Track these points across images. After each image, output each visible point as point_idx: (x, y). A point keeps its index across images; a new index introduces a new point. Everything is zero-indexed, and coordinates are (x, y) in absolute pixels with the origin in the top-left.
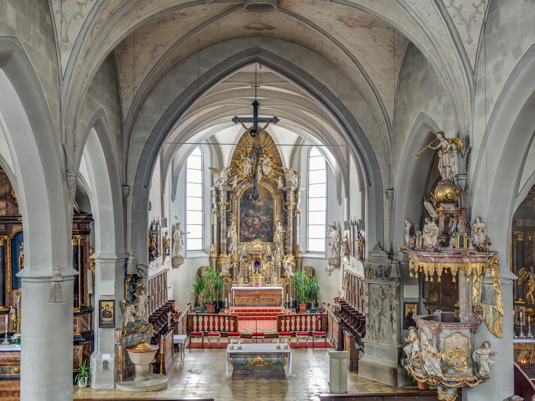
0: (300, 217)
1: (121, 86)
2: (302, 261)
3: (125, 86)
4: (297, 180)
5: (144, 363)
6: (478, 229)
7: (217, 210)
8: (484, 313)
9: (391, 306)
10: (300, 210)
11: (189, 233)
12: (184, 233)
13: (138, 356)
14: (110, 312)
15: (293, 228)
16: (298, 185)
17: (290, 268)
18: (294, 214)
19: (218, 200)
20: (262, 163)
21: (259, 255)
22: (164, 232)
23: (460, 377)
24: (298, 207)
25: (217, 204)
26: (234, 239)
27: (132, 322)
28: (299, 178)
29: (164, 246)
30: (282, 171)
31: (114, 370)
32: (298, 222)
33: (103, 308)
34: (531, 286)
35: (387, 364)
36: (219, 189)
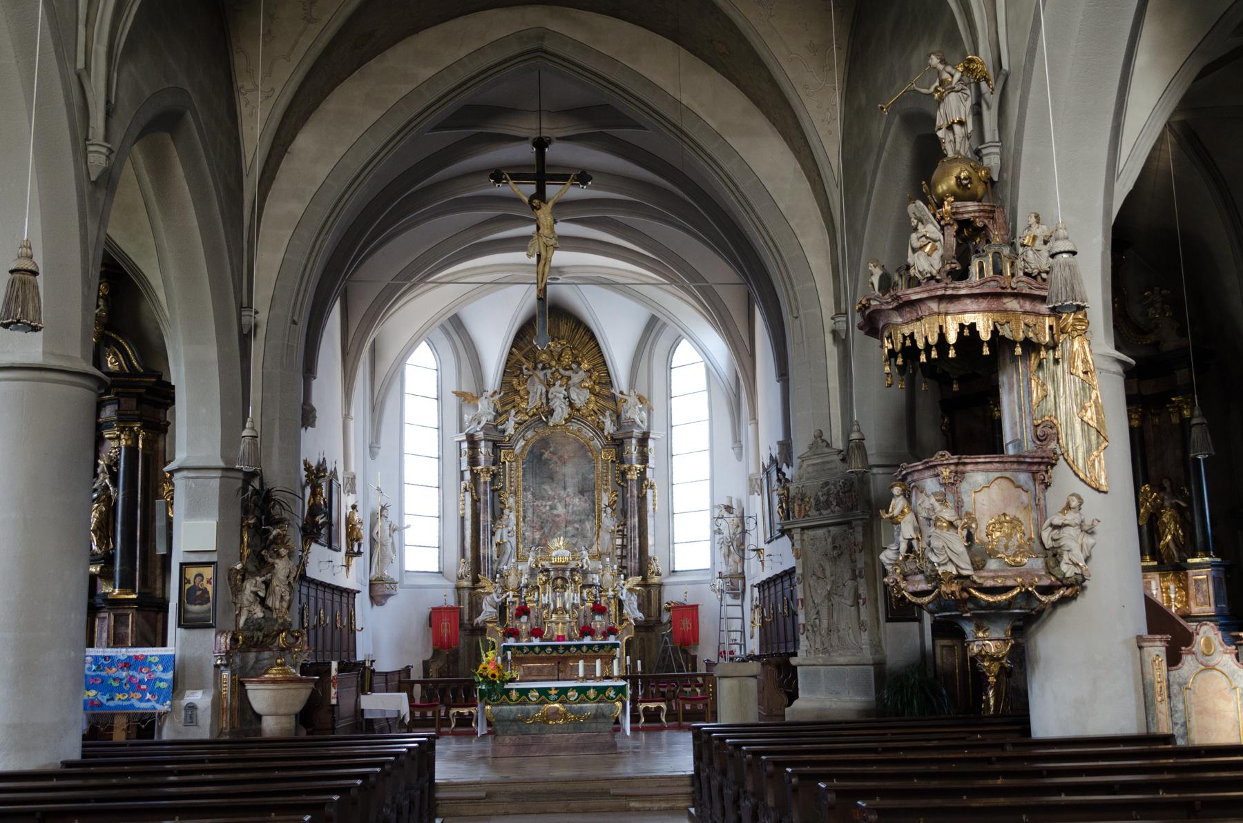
0: (654, 496)
1: (239, 84)
2: (660, 592)
4: (644, 415)
5: (282, 711)
6: (1035, 238)
7: (472, 485)
8: (1062, 436)
9: (854, 571)
10: (654, 481)
11: (408, 527)
12: (397, 529)
13: (267, 692)
14: (205, 591)
15: (639, 522)
16: (649, 426)
17: (634, 598)
18: (640, 489)
19: (473, 461)
20: (570, 382)
21: (564, 570)
22: (350, 505)
23: (1017, 576)
24: (649, 473)
25: (472, 471)
26: (508, 546)
27: (258, 618)
28: (650, 411)
29: (348, 535)
30: (613, 397)
31: (212, 725)
32: (650, 507)
33: (189, 582)
34: (1168, 523)
35: (851, 705)
36: (476, 438)
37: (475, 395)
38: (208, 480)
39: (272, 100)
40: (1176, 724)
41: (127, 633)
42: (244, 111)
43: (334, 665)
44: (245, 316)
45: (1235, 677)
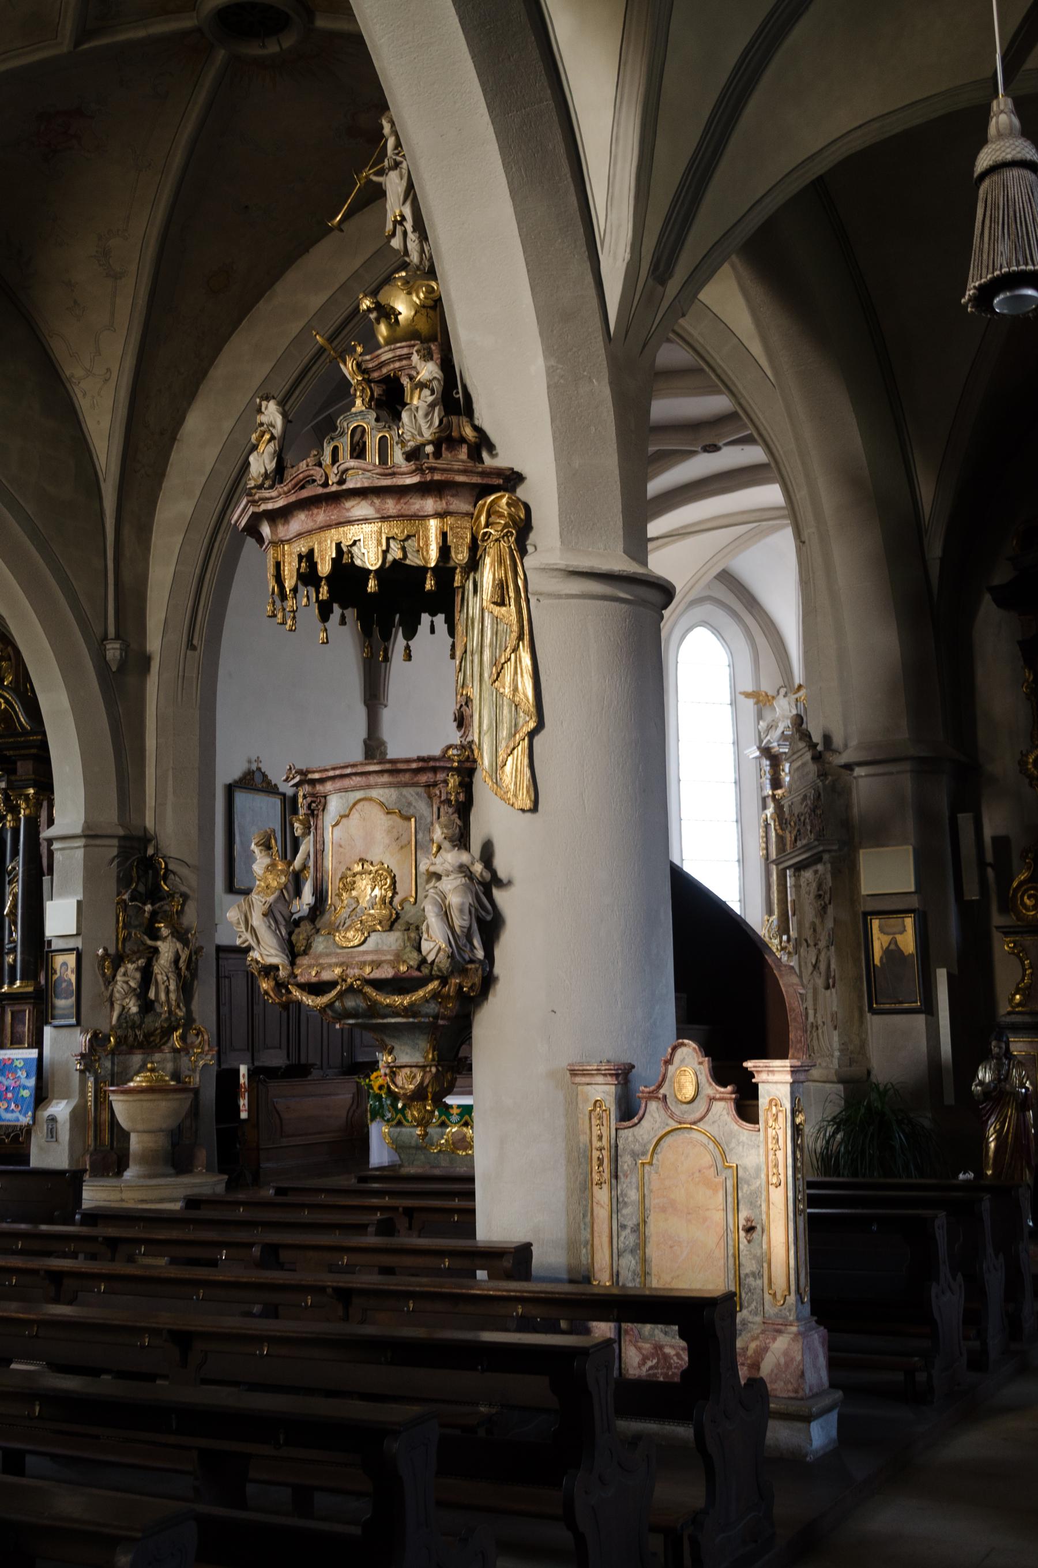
1: (68, 373)
3: (79, 372)
37: (770, 693)
38: (73, 851)
39: (112, 384)
40: (623, 1227)
41: (24, 1032)
42: (83, 404)
43: (243, 1069)
44: (109, 649)
45: (733, 1145)
